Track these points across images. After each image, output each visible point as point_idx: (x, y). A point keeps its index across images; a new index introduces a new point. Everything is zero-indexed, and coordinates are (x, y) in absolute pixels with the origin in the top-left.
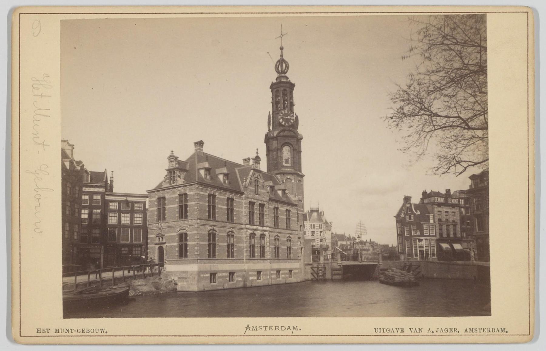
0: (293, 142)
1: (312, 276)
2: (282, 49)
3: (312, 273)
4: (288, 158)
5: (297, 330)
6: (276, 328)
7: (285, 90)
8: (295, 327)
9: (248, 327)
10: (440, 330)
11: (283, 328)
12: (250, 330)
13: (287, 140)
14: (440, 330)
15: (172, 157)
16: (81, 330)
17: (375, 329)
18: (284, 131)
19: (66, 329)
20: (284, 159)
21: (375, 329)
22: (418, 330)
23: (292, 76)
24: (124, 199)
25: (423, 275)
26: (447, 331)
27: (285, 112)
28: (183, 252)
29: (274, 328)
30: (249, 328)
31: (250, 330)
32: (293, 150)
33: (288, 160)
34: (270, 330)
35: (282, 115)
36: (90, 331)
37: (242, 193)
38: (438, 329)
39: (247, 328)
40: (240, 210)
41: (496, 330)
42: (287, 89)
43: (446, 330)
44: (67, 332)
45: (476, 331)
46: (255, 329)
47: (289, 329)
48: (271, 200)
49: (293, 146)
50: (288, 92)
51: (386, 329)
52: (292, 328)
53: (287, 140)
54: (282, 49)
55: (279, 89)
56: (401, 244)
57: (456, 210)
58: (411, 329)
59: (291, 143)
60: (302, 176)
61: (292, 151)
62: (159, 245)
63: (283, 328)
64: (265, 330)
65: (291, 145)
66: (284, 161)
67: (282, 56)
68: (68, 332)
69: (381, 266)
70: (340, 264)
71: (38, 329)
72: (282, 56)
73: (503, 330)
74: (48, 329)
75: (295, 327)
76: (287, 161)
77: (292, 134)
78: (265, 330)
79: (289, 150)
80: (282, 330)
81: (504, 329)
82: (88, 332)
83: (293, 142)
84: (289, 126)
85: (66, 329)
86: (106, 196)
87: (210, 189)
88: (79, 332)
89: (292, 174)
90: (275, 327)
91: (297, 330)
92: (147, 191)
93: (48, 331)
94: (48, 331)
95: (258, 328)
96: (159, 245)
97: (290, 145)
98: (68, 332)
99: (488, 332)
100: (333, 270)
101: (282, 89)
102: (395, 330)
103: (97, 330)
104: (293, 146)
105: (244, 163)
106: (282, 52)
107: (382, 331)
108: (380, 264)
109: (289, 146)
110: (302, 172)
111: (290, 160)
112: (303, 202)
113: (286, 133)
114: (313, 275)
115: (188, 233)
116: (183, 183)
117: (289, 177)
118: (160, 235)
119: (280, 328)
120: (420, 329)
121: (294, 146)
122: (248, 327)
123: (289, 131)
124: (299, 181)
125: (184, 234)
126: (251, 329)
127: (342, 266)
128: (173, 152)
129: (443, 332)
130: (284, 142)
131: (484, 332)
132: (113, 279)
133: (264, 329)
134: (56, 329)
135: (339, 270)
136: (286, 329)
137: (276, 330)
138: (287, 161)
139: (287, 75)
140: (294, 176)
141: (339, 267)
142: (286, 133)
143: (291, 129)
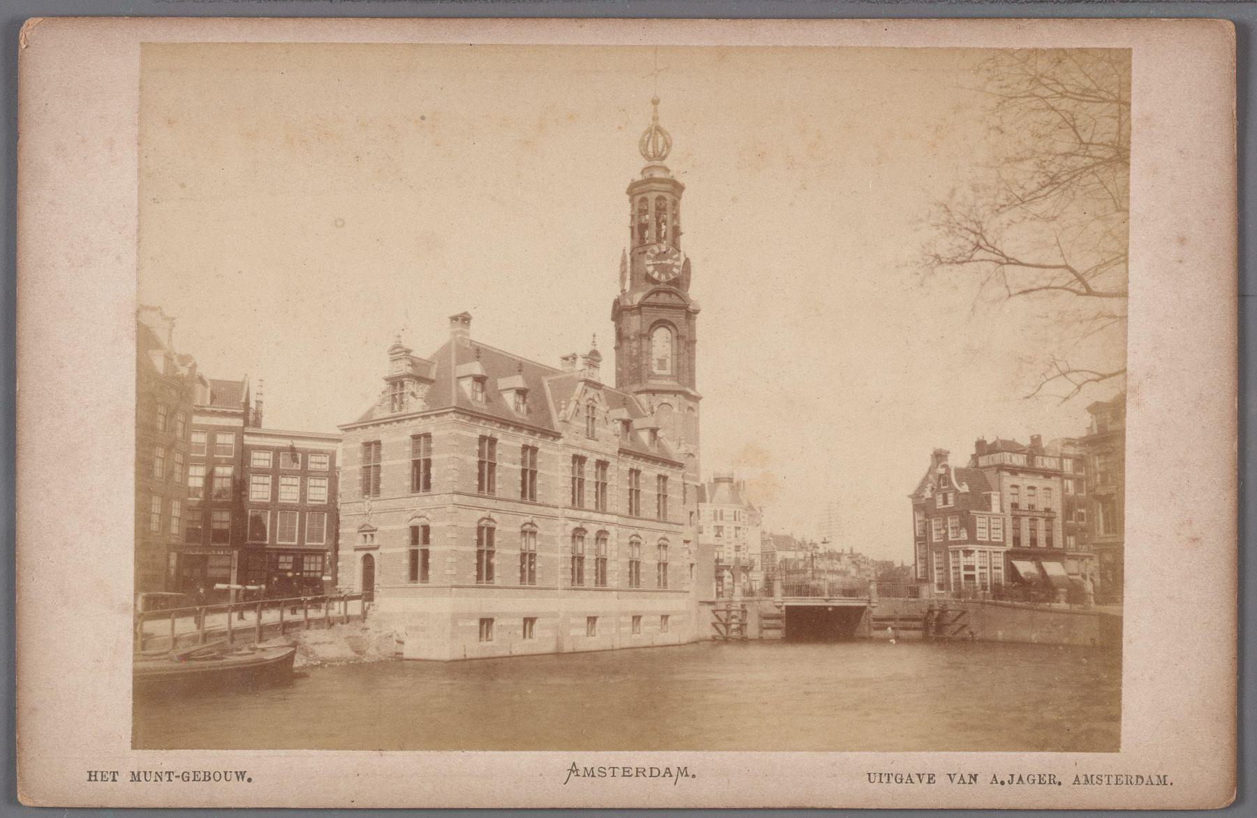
2: (655, 102)
3: (714, 625)
5: (687, 775)
6: (637, 771)
7: (659, 198)
8: (589, 770)
10: (1016, 778)
11: (655, 772)
13: (664, 315)
14: (1016, 778)
15: (397, 350)
16: (1037, 778)
17: (869, 774)
18: (657, 292)
19: (156, 773)
20: (654, 357)
22: (967, 779)
23: (675, 167)
28: (419, 566)
29: (634, 772)
30: (577, 770)
31: (578, 775)
32: (678, 337)
33: (665, 360)
34: (624, 776)
36: (211, 776)
37: (557, 436)
38: (1012, 776)
39: (571, 770)
41: (905, 778)
42: (668, 196)
43: (1031, 777)
45: (1099, 782)
46: (590, 773)
48: (623, 452)
49: (677, 331)
52: (674, 772)
53: (664, 315)
54: (655, 102)
58: (952, 776)
59: (674, 321)
60: (697, 399)
65: (673, 325)
66: (655, 362)
67: (655, 119)
70: (780, 604)
71: (90, 772)
72: (655, 119)
73: (241, 775)
74: (169, 773)
75: (136, 774)
76: (662, 363)
77: (675, 300)
79: (667, 338)
80: (651, 776)
81: (1164, 777)
82: (207, 779)
83: (678, 317)
84: (668, 283)
87: (484, 424)
88: (186, 779)
89: (675, 393)
90: (624, 768)
92: (338, 427)
93: (114, 777)
94: (114, 777)
97: (670, 327)
101: (655, 195)
102: (916, 779)
103: (228, 774)
104: (677, 331)
106: (656, 111)
107: (884, 779)
108: (872, 605)
109: (667, 328)
111: (668, 361)
112: (697, 458)
113: (663, 299)
114: (718, 629)
115: (431, 525)
117: (665, 400)
119: (648, 773)
120: (971, 776)
122: (574, 769)
123: (670, 293)
124: (690, 408)
125: (422, 526)
126: (581, 772)
127: (783, 608)
133: (609, 772)
134: (1159, 776)
135: (778, 617)
136: (662, 774)
137: (637, 776)
138: (662, 363)
139: (666, 163)
141: (777, 611)
142: (663, 299)
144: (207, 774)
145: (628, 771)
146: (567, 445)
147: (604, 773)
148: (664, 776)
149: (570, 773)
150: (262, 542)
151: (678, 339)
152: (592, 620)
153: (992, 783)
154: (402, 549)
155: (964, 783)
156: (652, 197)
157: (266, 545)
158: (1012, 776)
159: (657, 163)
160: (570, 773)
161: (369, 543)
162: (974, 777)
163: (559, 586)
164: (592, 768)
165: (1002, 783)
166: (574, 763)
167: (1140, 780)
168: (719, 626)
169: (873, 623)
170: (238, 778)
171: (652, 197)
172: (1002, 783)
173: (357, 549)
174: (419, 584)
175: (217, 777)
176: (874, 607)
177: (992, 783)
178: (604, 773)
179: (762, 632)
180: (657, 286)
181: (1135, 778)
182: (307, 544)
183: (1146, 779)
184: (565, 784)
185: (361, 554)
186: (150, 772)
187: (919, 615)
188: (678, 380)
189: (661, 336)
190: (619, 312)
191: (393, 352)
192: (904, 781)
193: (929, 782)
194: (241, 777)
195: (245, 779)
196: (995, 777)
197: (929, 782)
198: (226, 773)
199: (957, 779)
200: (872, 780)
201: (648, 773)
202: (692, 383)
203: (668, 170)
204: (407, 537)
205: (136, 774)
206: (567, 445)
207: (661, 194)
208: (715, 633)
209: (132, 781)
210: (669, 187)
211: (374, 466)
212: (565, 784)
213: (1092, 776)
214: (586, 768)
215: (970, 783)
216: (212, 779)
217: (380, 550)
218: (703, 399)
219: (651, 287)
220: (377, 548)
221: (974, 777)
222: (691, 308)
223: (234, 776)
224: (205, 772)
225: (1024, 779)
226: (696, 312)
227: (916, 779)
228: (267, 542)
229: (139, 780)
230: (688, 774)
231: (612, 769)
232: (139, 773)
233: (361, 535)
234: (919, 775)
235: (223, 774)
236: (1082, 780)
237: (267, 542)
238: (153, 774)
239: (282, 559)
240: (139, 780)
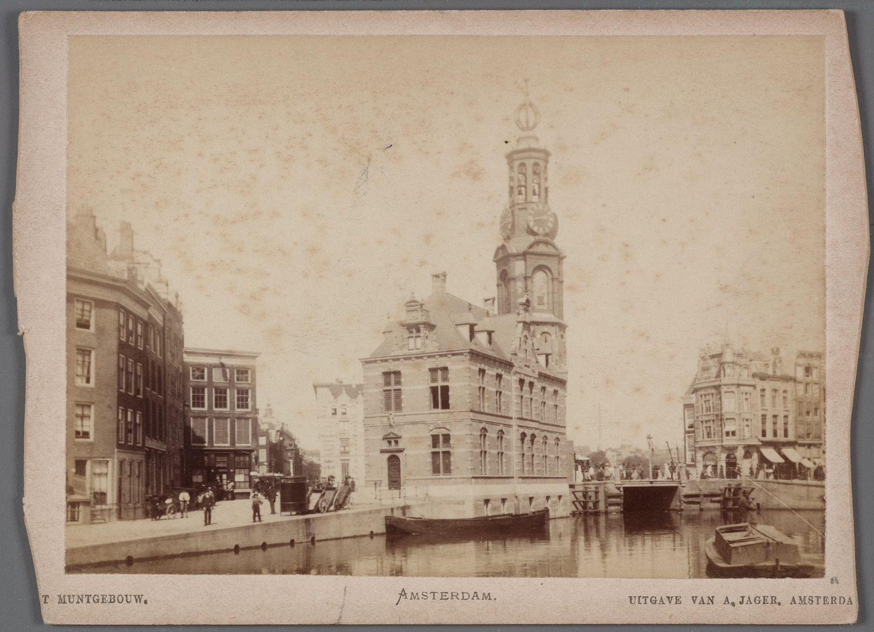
0: (552, 263)
1: (574, 506)
3: (573, 502)
4: (544, 294)
5: (490, 599)
6: (452, 596)
7: (536, 164)
8: (486, 595)
9: (403, 593)
10: (746, 600)
12: (406, 598)
13: (542, 261)
15: (413, 304)
18: (537, 243)
19: (78, 596)
21: (631, 597)
24: (214, 361)
25: (758, 505)
26: (760, 601)
27: (538, 206)
30: (405, 594)
31: (406, 598)
32: (553, 279)
33: (543, 297)
34: (442, 599)
35: (533, 212)
36: (116, 598)
39: (401, 594)
40: (509, 393)
42: (541, 163)
44: (79, 601)
47: (475, 598)
49: (552, 273)
50: (542, 168)
51: (650, 598)
53: (542, 261)
55: (527, 162)
56: (187, 403)
57: (789, 386)
59: (549, 265)
61: (550, 281)
62: (390, 454)
63: (466, 596)
64: (434, 599)
65: (550, 270)
68: (713, 603)
69: (685, 488)
70: (619, 486)
73: (138, 598)
78: (434, 599)
82: (112, 600)
83: (552, 263)
85: (78, 596)
86: (185, 356)
88: (757, 602)
89: (553, 324)
90: (442, 593)
91: (490, 599)
92: (360, 359)
93: (45, 599)
94: (45, 599)
95: (420, 595)
96: (390, 454)
98: (713, 603)
99: (772, 603)
100: (609, 496)
101: (532, 161)
104: (552, 273)
105: (485, 306)
107: (642, 600)
108: (683, 485)
109: (542, 270)
110: (564, 320)
113: (541, 248)
114: (575, 505)
115: (451, 434)
116: (437, 350)
118: (391, 436)
119: (460, 597)
121: (553, 271)
122: (403, 593)
123: (547, 243)
125: (443, 435)
126: (480, 597)
127: (622, 489)
128: (415, 295)
129: (751, 603)
130: (537, 264)
131: (824, 604)
132: (598, 510)
135: (618, 496)
137: (452, 598)
140: (554, 328)
141: (616, 492)
142: (541, 248)
143: (549, 239)
144: (112, 597)
145: (445, 596)
146: (517, 373)
147: (424, 595)
148: (473, 599)
149: (400, 597)
150: (202, 445)
151: (553, 281)
152: (531, 499)
153: (791, 604)
154: (425, 450)
155: (704, 603)
156: (529, 163)
157: (205, 447)
158: (743, 597)
159: (530, 133)
160: (400, 597)
161: (393, 446)
162: (711, 600)
163: (515, 476)
164: (417, 593)
165: (733, 604)
166: (489, 593)
167: (842, 600)
168: (577, 504)
169: (683, 499)
170: (137, 601)
171: (529, 163)
172: (733, 604)
173: (382, 451)
174: (441, 476)
175: (120, 598)
176: (683, 487)
177: (791, 604)
178: (424, 595)
179: (607, 507)
180: (537, 238)
181: (838, 598)
182: (237, 445)
183: (648, 600)
184: (397, 604)
185: (387, 455)
186: (635, 597)
187: (719, 492)
188: (553, 314)
189: (540, 276)
190: (503, 259)
191: (408, 305)
192: (658, 602)
193: (676, 603)
194: (138, 600)
195: (142, 602)
196: (727, 598)
197: (676, 603)
198: (126, 596)
199: (698, 600)
200: (633, 602)
201: (460, 597)
202: (561, 316)
203: (537, 140)
204: (430, 442)
205: (62, 597)
206: (517, 373)
207: (537, 161)
208: (574, 509)
209: (59, 603)
210: (542, 155)
211: (394, 390)
212: (397, 604)
213: (805, 597)
214: (412, 593)
215: (708, 604)
216: (117, 601)
217: (405, 452)
218: (496, 332)
219: (532, 239)
220: (401, 451)
221: (711, 600)
222: (561, 255)
223: (133, 598)
224: (111, 596)
225: (752, 600)
226: (564, 257)
227: (666, 601)
228: (206, 445)
229: (65, 602)
230: (491, 598)
231: (44, 597)
232: (64, 596)
233: (386, 441)
234: (668, 597)
235: (125, 598)
236: (797, 600)
237: (206, 445)
238: (76, 597)
239: (219, 459)
240: (65, 602)
